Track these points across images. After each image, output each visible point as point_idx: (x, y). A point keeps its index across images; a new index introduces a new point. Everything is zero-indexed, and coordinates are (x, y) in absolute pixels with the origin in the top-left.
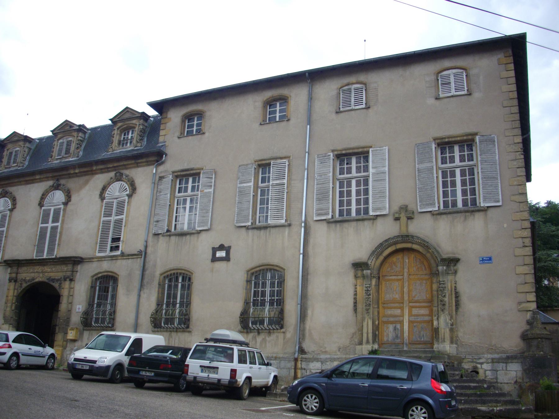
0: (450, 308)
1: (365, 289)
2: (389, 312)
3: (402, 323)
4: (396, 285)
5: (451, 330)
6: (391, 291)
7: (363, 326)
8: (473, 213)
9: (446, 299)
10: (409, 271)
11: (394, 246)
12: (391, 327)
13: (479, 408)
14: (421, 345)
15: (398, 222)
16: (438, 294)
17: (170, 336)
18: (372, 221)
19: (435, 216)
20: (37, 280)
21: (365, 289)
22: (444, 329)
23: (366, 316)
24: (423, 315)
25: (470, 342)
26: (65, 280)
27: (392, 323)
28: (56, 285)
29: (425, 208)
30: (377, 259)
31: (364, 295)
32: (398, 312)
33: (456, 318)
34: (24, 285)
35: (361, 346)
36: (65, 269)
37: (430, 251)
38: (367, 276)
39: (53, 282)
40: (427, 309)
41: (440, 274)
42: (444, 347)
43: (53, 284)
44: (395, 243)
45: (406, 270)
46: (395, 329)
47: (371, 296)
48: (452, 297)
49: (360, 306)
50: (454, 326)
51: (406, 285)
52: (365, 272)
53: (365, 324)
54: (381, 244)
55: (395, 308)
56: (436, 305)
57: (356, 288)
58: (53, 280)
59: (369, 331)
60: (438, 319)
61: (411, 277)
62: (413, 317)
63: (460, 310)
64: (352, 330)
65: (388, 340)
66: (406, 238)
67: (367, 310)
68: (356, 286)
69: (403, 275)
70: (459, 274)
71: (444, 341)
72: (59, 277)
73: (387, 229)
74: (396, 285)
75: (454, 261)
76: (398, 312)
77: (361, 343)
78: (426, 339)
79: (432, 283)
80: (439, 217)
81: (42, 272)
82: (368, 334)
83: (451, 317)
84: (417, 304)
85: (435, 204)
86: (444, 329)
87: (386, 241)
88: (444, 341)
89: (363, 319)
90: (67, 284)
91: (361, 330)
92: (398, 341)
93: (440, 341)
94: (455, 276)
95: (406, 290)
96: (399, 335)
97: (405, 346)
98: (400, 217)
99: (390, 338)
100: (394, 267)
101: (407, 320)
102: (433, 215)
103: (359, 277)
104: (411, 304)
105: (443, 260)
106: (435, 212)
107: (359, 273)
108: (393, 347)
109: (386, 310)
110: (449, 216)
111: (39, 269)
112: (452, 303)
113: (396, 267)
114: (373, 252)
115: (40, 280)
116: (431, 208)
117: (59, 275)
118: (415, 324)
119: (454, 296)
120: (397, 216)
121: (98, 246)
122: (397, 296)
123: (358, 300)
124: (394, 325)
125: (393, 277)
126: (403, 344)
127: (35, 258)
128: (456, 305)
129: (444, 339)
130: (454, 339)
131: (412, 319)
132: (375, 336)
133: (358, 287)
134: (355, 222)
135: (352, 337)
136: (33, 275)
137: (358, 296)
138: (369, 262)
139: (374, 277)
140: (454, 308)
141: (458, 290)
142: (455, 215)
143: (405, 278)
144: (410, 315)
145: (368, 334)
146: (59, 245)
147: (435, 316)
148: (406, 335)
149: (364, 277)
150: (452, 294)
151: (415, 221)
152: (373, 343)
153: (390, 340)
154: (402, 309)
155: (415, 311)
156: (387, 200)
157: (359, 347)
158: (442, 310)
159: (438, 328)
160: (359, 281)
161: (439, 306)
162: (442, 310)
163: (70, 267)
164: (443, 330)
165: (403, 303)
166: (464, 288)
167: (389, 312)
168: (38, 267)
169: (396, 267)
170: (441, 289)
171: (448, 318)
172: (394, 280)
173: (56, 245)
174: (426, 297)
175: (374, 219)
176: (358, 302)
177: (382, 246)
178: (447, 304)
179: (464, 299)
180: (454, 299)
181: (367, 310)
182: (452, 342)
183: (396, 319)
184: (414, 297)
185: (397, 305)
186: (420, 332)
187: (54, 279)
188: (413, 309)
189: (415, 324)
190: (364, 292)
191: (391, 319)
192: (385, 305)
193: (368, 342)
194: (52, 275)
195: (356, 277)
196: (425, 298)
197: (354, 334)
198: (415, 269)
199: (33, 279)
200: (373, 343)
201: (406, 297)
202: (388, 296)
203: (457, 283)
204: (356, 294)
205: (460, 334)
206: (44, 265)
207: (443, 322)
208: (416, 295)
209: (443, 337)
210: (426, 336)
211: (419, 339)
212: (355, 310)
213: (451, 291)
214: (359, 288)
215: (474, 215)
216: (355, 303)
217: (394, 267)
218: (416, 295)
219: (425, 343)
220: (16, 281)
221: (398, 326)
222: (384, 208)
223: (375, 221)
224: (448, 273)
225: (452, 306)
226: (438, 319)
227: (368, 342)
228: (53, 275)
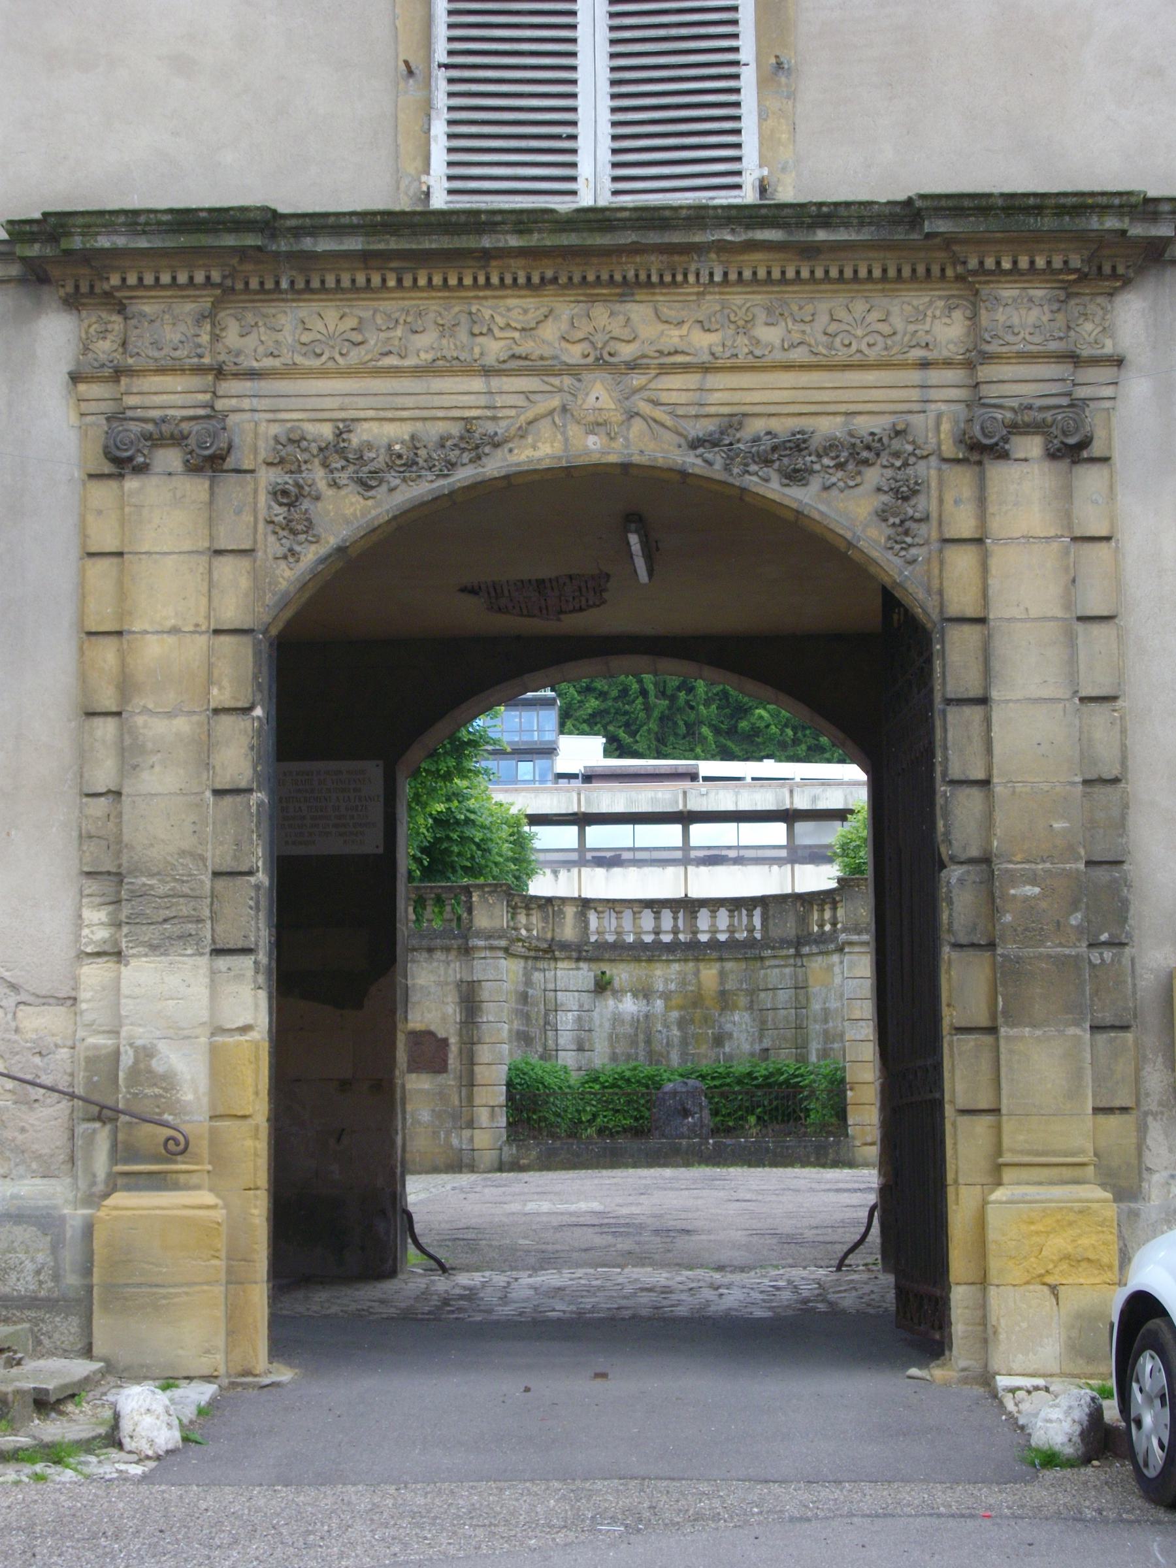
17: (737, 794)
20: (541, 450)
26: (982, 449)
28: (849, 510)
34: (346, 514)
36: (770, 335)
39: (795, 476)
43: (804, 497)
58: (792, 454)
72: (877, 425)
81: (602, 363)
90: (1024, 489)
111: (555, 324)
115: (594, 447)
117: (863, 400)
121: (439, 128)
127: (439, 201)
136: (463, 394)
146: (776, 71)
163: (1022, 312)
168: (518, 308)
173: (748, 78)
187: (798, 444)
194: (727, 392)
199: (473, 441)
206: (628, 288)
220: (212, 462)
228: (773, 400)
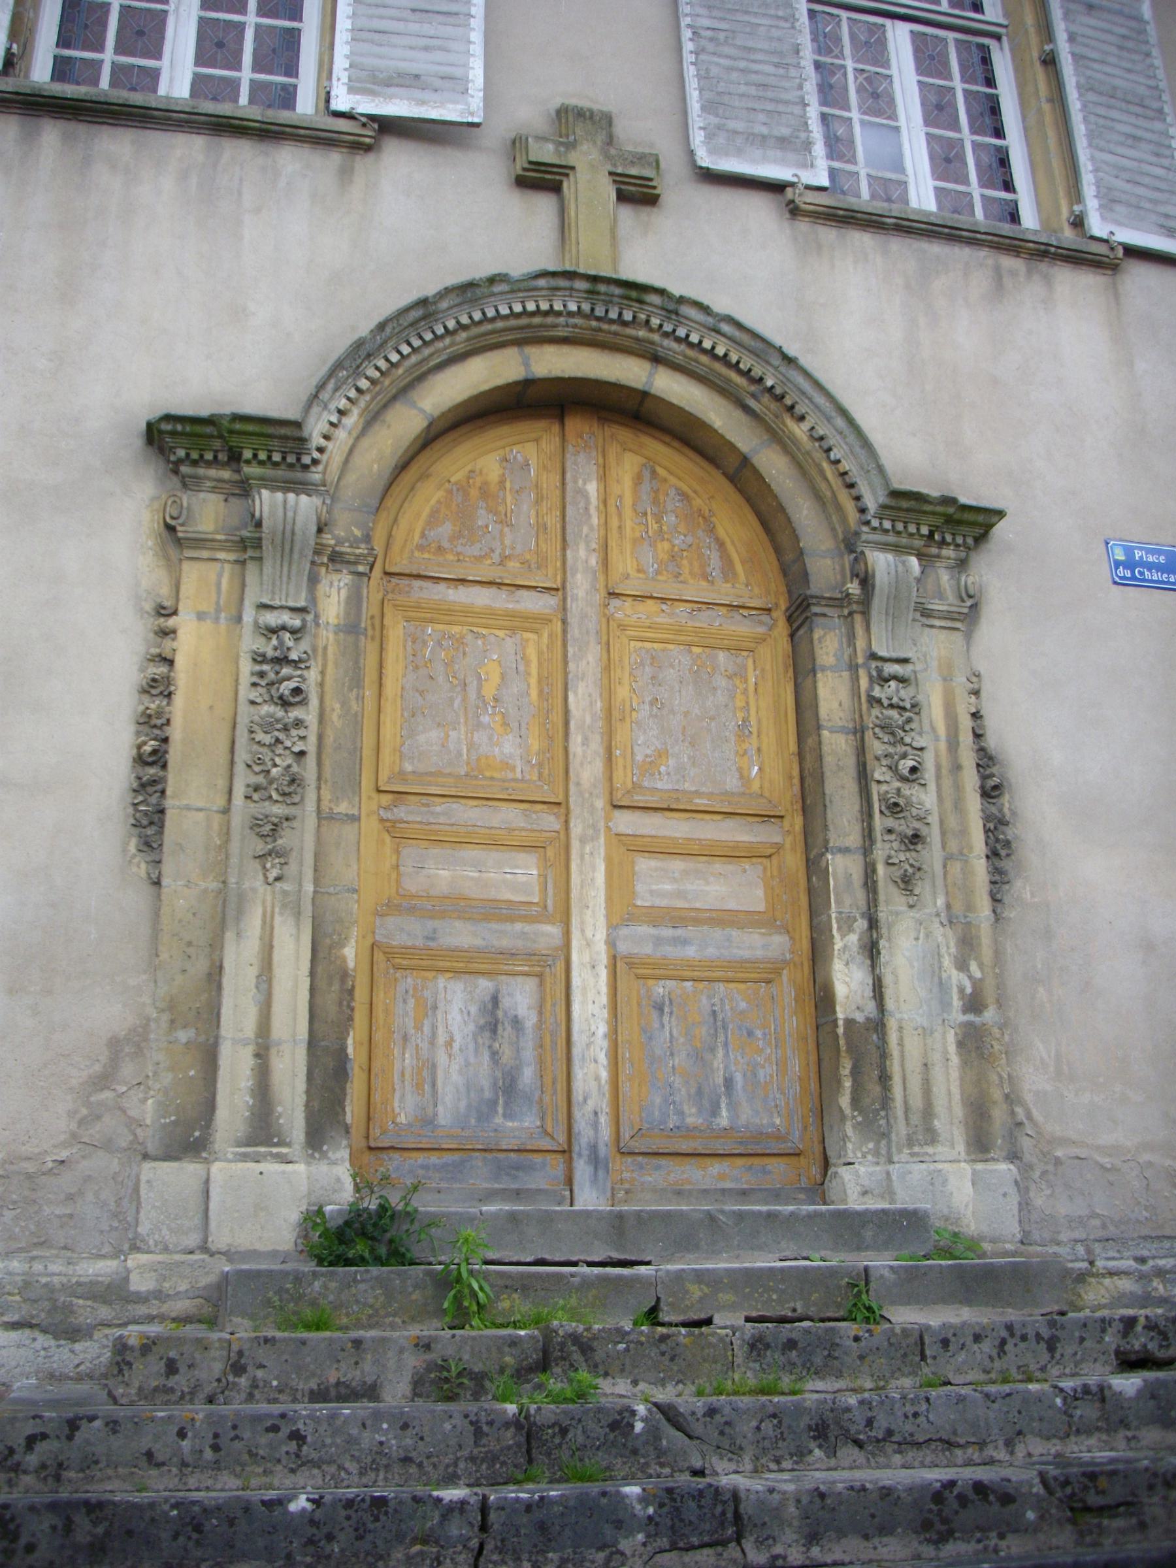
0: (956, 868)
1: (250, 642)
2: (443, 873)
3: (553, 971)
4: (501, 663)
5: (973, 1043)
6: (464, 698)
7: (215, 976)
8: (1043, 266)
9: (926, 798)
10: (605, 563)
11: (512, 352)
12: (456, 1005)
13: (435, 1493)
14: (716, 1168)
15: (544, 203)
16: (861, 751)
18: (335, 158)
19: (803, 225)
21: (250, 642)
22: (926, 1032)
23: (254, 882)
24: (722, 919)
25: (1106, 1139)
27: (464, 964)
29: (739, 153)
30: (372, 419)
31: (246, 692)
32: (519, 876)
33: (998, 954)
35: (188, 1171)
37: (800, 431)
38: (287, 541)
40: (752, 871)
41: (878, 604)
42: (936, 1181)
44: (530, 333)
45: (583, 555)
46: (492, 1019)
47: (309, 714)
48: (958, 787)
49: (192, 791)
50: (990, 1015)
51: (586, 663)
52: (267, 501)
53: (240, 959)
54: (425, 309)
55: (492, 842)
56: (854, 839)
57: (166, 633)
59: (280, 1028)
60: (872, 950)
61: (624, 610)
62: (644, 930)
63: (1021, 889)
64: (107, 1012)
65: (429, 1121)
66: (623, 307)
67: (269, 830)
68: (164, 611)
69: (559, 590)
70: (995, 629)
71: (932, 1137)
73: (454, 227)
74: (501, 663)
75: (956, 526)
76: (519, 876)
77: (189, 1139)
78: (748, 1113)
79: (802, 669)
80: (828, 234)
82: (262, 1055)
83: (967, 944)
84: (677, 828)
85: (808, 145)
86: (926, 1032)
87: (467, 291)
88: (932, 1137)
89: (224, 913)
91: (199, 1010)
92: (520, 1126)
93: (901, 1129)
94: (968, 636)
95: (584, 701)
96: (528, 1075)
97: (582, 1169)
98: (566, 170)
99: (450, 1105)
100: (483, 517)
101: (601, 948)
102: (794, 211)
103: (199, 542)
104: (626, 822)
105: (905, 504)
106: (811, 197)
107: (209, 512)
108: (480, 1177)
109: (410, 853)
110: (897, 244)
112: (964, 832)
113: (504, 521)
114: (359, 354)
116: (783, 162)
118: (660, 989)
119: (971, 780)
120: (546, 153)
122: (511, 750)
123: (176, 733)
124: (485, 985)
125: (481, 597)
126: (567, 1152)
128: (993, 854)
129: (928, 1112)
130: (999, 1114)
131: (640, 940)
132: (329, 1072)
133: (185, 623)
134: (198, 142)
135: (103, 1080)
137: (179, 708)
138: (315, 430)
139: (336, 558)
140: (980, 866)
141: (991, 742)
142: (936, 249)
143: (574, 608)
144: (624, 911)
145: (262, 1055)
147: (847, 925)
148: (592, 1072)
149: (249, 543)
150: (957, 768)
151: (663, 220)
152: (316, 1139)
153: (444, 1116)
154: (556, 854)
155: (657, 882)
156: (477, 37)
157: (171, 1179)
158: (906, 883)
159: (878, 1025)
160: (204, 582)
161: (880, 852)
162: (906, 883)
164: (913, 1046)
165: (560, 806)
166: (1029, 734)
167: (443, 873)
169: (504, 521)
170: (888, 708)
171: (946, 940)
172: (489, 617)
174: (744, 777)
175: (359, 147)
176: (174, 755)
177: (427, 327)
178: (934, 835)
179: (1037, 809)
180: (974, 804)
181: (269, 830)
182: (980, 1144)
183: (507, 936)
184: (650, 766)
185: (511, 815)
186: (700, 1057)
188: (644, 864)
189: (660, 989)
190: (246, 667)
191: (461, 935)
192: (401, 812)
193: (262, 1131)
195: (174, 536)
196: (732, 783)
197: (124, 1047)
198: (648, 558)
200: (316, 1139)
201: (588, 768)
202: (429, 737)
203: (986, 688)
204: (159, 688)
205: (1034, 1081)
207: (911, 976)
208: (662, 754)
209: (917, 1102)
210: (760, 1083)
211: (693, 1119)
212: (149, 818)
213: (953, 744)
214: (193, 640)
215: (1048, 281)
216: (152, 761)
217: (483, 517)
218: (662, 754)
219: (752, 1149)
221: (521, 998)
222: (457, 84)
223: (362, 162)
224: (926, 613)
225: (962, 856)
226: (872, 950)
227: (262, 1131)
